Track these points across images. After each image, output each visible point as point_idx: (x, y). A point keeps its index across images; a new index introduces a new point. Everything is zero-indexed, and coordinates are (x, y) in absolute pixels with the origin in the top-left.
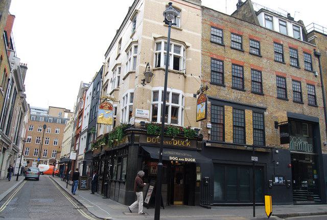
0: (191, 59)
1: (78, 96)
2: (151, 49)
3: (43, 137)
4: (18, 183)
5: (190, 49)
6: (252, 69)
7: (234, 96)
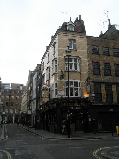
0: (82, 64)
1: (28, 79)
2: (63, 62)
3: (10, 102)
4: (3, 129)
5: (82, 59)
6: (115, 64)
7: (106, 79)
